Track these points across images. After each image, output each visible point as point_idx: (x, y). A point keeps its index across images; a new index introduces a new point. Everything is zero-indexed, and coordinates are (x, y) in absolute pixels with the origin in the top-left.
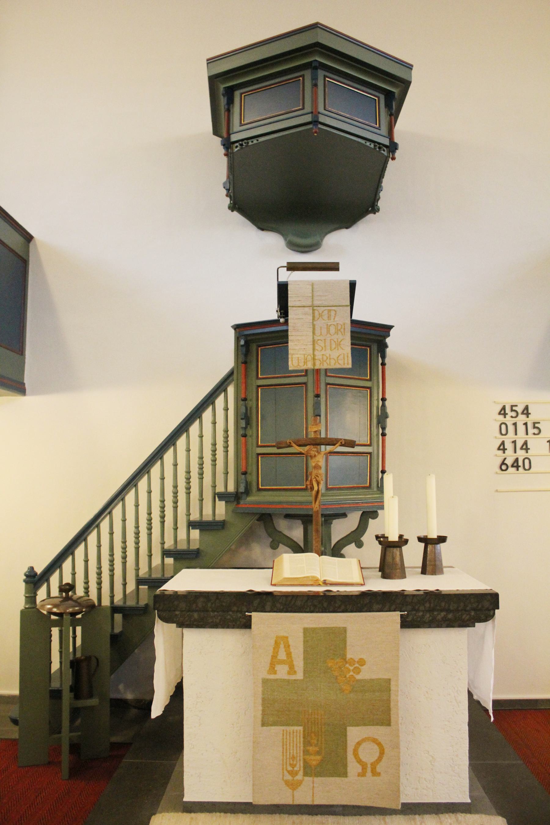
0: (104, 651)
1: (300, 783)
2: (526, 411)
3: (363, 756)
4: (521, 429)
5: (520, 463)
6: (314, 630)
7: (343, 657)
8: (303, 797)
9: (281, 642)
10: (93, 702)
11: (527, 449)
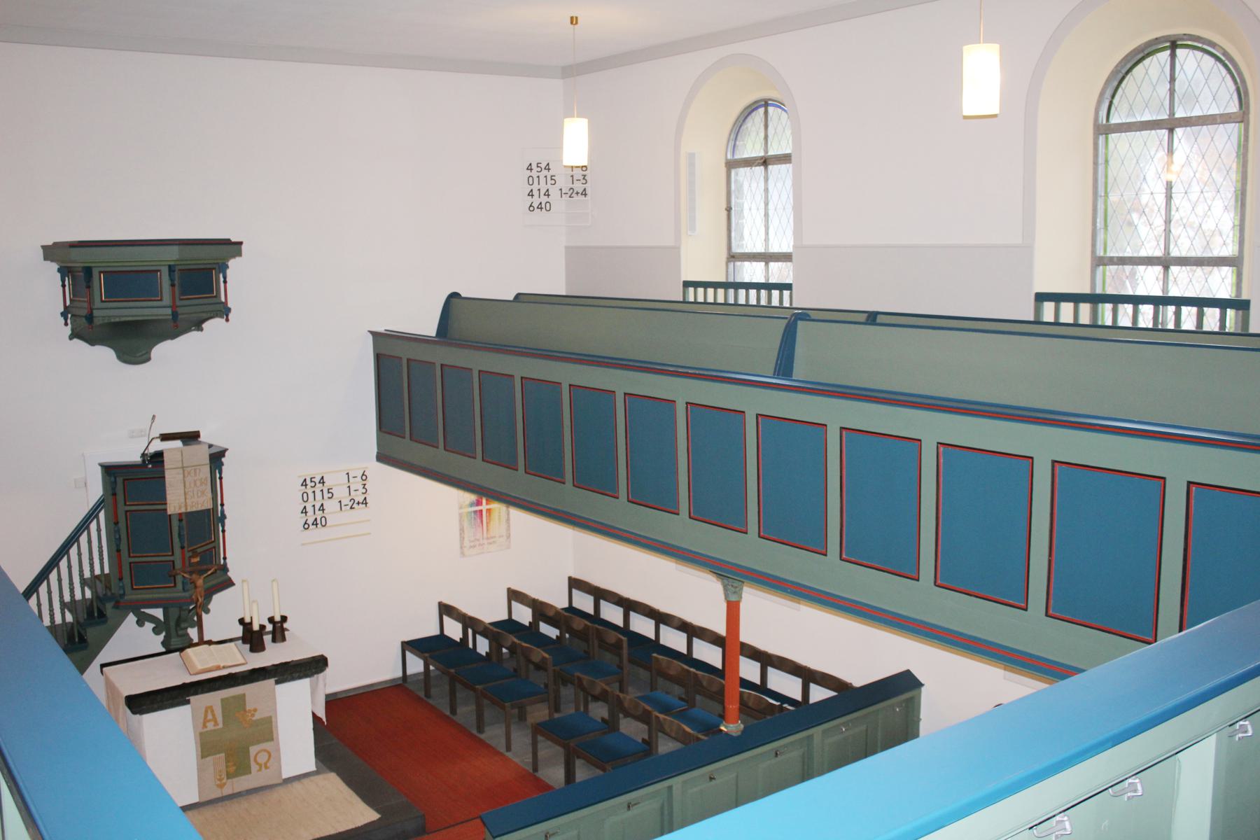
2: (322, 481)
4: (319, 494)
8: (227, 791)
9: (209, 709)
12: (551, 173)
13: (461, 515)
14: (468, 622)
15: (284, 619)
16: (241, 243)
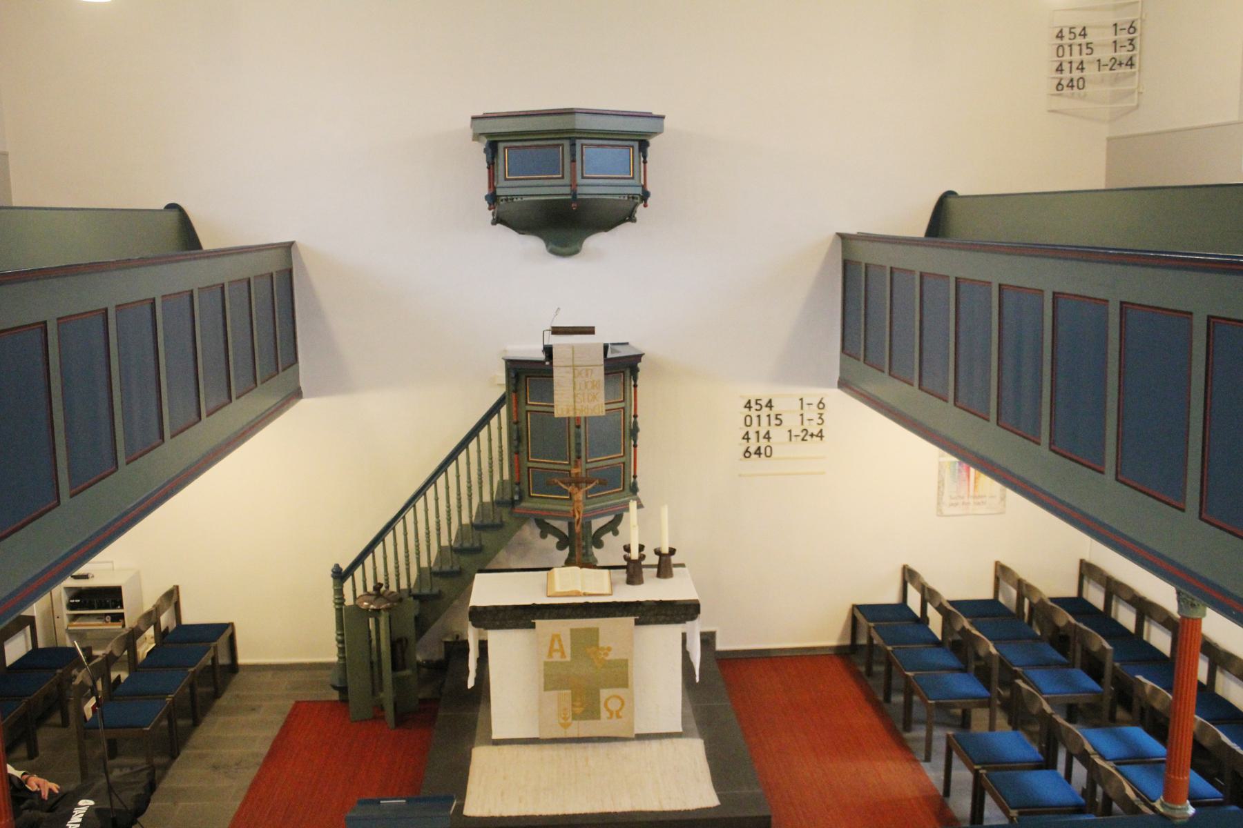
0: (410, 632)
1: (569, 725)
2: (770, 405)
3: (610, 706)
4: (764, 420)
5: (762, 451)
6: (577, 630)
7: (597, 645)
8: (573, 732)
9: (556, 638)
10: (408, 672)
11: (769, 438)
12: (1088, 40)
13: (940, 464)
14: (928, 595)
15: (672, 551)
16: (663, 117)
